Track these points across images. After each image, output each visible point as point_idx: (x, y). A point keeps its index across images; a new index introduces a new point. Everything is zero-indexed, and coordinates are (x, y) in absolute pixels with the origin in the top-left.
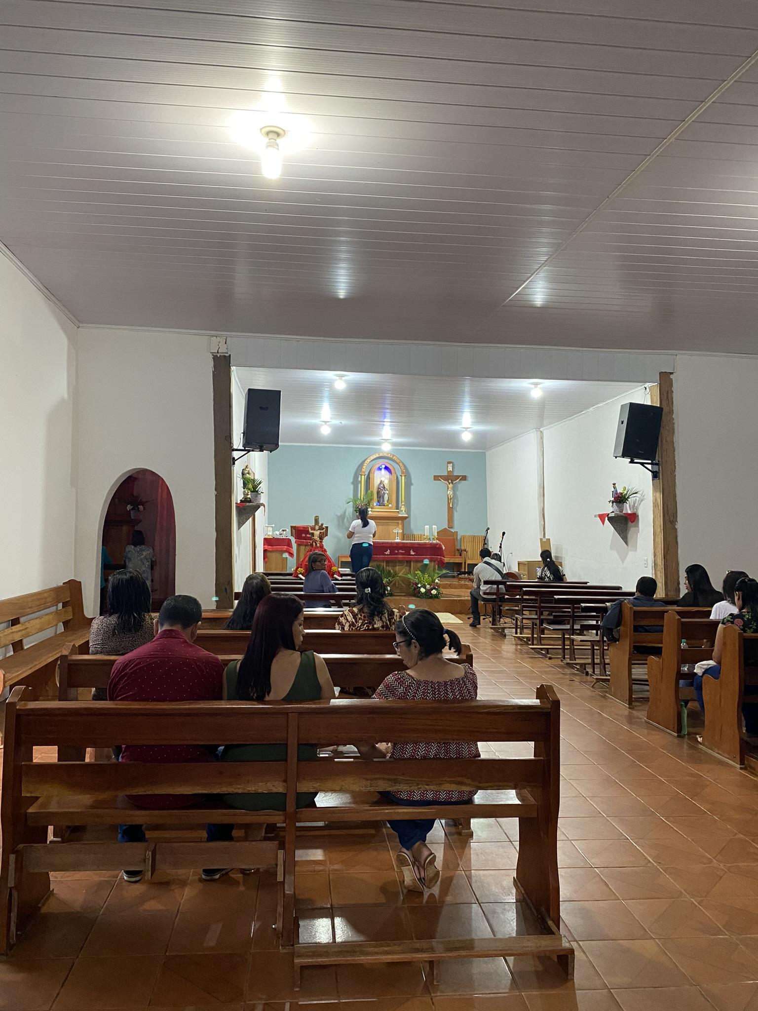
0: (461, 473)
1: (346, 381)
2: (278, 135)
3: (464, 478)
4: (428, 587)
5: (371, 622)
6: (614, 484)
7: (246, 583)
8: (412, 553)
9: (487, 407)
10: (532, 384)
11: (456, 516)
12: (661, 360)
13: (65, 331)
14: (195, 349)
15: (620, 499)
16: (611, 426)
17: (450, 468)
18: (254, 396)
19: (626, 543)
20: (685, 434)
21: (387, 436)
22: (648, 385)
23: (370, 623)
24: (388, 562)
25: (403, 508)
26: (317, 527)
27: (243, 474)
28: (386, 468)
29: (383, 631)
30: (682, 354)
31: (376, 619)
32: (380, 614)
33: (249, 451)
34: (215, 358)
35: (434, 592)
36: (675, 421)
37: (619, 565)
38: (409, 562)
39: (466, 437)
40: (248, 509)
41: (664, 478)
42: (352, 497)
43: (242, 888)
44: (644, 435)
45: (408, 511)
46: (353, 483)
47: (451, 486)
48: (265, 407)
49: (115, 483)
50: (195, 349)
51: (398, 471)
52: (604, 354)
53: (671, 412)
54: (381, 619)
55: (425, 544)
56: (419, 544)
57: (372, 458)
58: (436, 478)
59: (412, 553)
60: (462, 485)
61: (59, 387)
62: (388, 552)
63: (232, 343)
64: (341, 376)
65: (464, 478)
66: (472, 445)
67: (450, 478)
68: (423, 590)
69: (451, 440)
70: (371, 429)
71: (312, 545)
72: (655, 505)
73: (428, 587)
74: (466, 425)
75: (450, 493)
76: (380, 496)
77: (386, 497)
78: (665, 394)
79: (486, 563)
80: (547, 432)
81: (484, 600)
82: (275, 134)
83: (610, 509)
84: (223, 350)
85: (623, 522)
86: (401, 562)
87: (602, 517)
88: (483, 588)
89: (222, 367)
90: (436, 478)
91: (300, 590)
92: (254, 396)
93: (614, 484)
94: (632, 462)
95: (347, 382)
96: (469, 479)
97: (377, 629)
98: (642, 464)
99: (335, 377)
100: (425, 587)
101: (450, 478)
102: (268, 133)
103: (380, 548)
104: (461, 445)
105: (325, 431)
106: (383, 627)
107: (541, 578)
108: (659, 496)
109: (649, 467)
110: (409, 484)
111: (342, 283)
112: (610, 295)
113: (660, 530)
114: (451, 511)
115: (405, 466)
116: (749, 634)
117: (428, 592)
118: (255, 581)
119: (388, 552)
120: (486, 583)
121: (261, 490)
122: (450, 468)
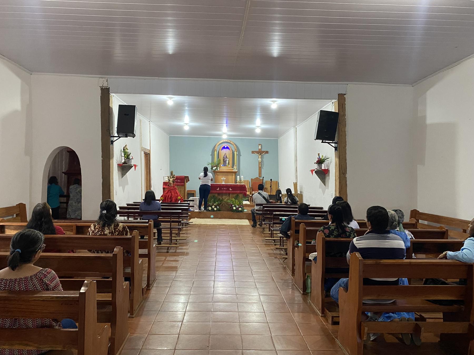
0: (266, 149)
1: (173, 101)
3: (267, 152)
4: (237, 206)
5: (103, 230)
6: (319, 154)
7: (34, 209)
8: (230, 189)
9: (268, 115)
10: (272, 101)
11: (263, 170)
12: (339, 87)
13: (18, 75)
14: (93, 84)
15: (320, 162)
17: (260, 148)
18: (121, 108)
19: (325, 185)
21: (225, 132)
22: (333, 101)
23: (102, 231)
24: (219, 194)
25: (235, 167)
26: (171, 177)
27: (124, 150)
28: (224, 148)
30: (351, 84)
31: (106, 228)
32: (109, 225)
33: (120, 137)
34: (102, 89)
35: (240, 209)
36: (347, 120)
38: (229, 194)
39: (258, 131)
42: (210, 162)
44: (329, 127)
46: (211, 155)
47: (260, 156)
48: (128, 113)
49: (51, 154)
50: (93, 84)
51: (232, 147)
52: (309, 84)
53: (344, 115)
54: (109, 228)
55: (238, 185)
56: (220, 185)
57: (220, 142)
58: (253, 152)
59: (230, 189)
60: (266, 156)
62: (218, 189)
63: (112, 81)
64: (171, 98)
65: (267, 152)
66: (261, 136)
67: (260, 152)
68: (234, 208)
70: (217, 127)
71: (169, 185)
72: (336, 165)
73: (237, 206)
74: (258, 125)
75: (260, 159)
76: (225, 162)
77: (227, 162)
78: (341, 106)
79: (259, 193)
81: (257, 214)
83: (316, 167)
84: (105, 85)
85: (322, 174)
86: (226, 194)
87: (312, 171)
88: (256, 208)
89: (105, 94)
90: (253, 152)
91: (138, 209)
92: (121, 108)
93: (319, 154)
94: (322, 142)
95: (173, 101)
96: (270, 152)
97: (106, 235)
98: (329, 143)
99: (168, 99)
100: (235, 207)
101: (260, 152)
103: (214, 187)
105: (186, 128)
106: (109, 233)
108: (337, 160)
109: (333, 145)
110: (239, 155)
111: (171, 43)
112: (308, 50)
113: (337, 178)
114: (260, 169)
115: (236, 145)
118: (38, 208)
119: (218, 189)
120: (257, 205)
121: (131, 157)
122: (260, 148)
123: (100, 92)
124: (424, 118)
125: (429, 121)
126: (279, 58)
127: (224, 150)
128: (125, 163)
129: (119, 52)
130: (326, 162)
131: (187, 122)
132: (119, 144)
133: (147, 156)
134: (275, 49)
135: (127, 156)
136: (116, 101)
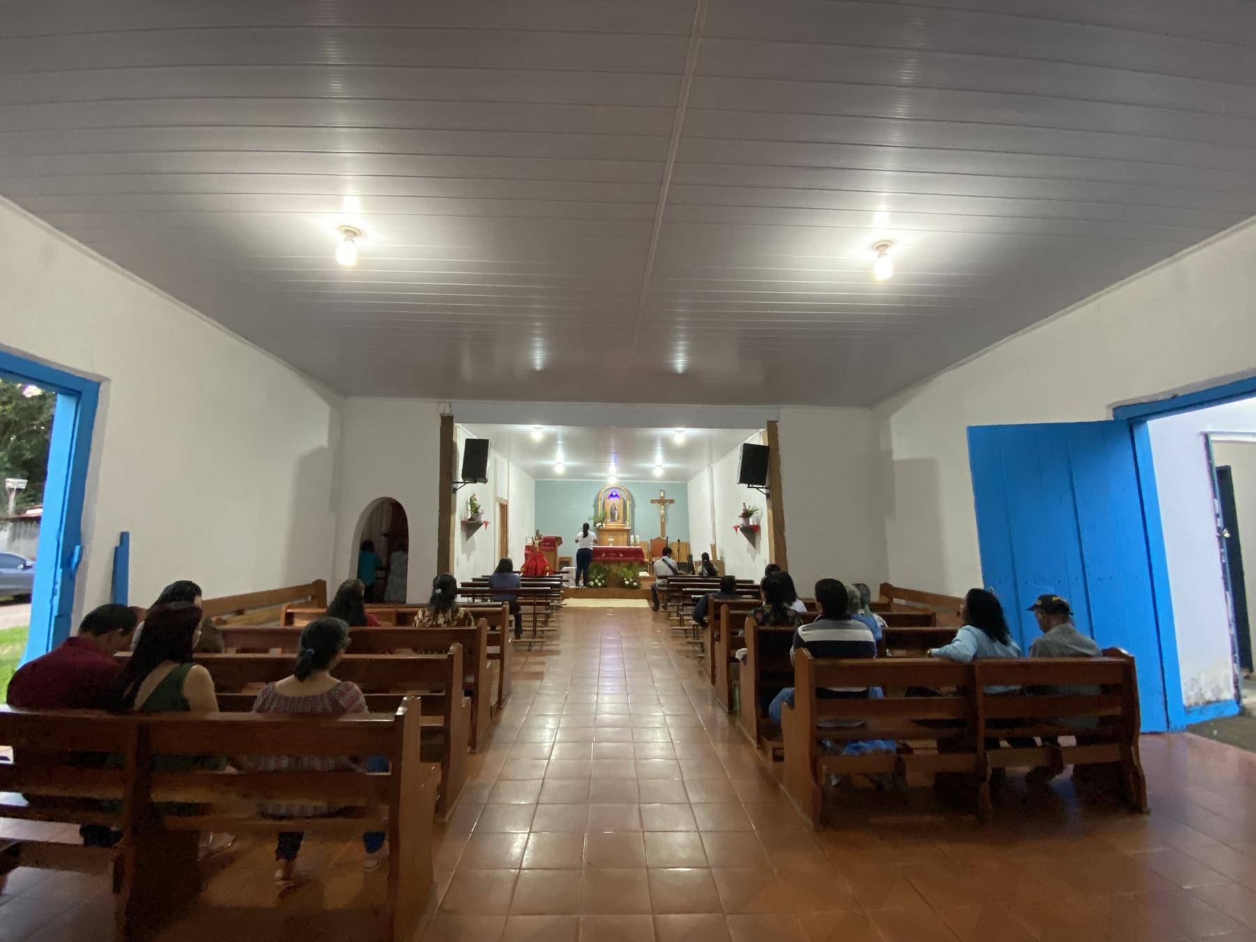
2: (355, 234)
3: (672, 501)
5: (435, 618)
12: (768, 412)
15: (747, 515)
16: (735, 460)
20: (789, 465)
21: (613, 474)
24: (604, 562)
29: (444, 627)
31: (440, 616)
32: (445, 611)
37: (748, 564)
40: (471, 526)
41: (775, 499)
43: (371, 863)
44: (757, 466)
45: (633, 524)
48: (478, 450)
50: (428, 412)
51: (623, 495)
58: (653, 501)
60: (671, 507)
61: (320, 438)
65: (672, 501)
67: (662, 501)
69: (646, 473)
74: (658, 465)
76: (613, 515)
80: (716, 468)
82: (352, 233)
83: (741, 522)
84: (448, 411)
85: (751, 532)
86: (614, 562)
87: (736, 528)
89: (447, 425)
90: (653, 501)
94: (1217, 516)
101: (662, 501)
102: (346, 231)
103: (598, 552)
104: (653, 478)
107: (701, 574)
110: (633, 506)
111: (538, 358)
114: (663, 524)
116: (767, 627)
117: (631, 584)
123: (439, 421)
124: (890, 452)
125: (896, 456)
126: (688, 373)
127: (612, 499)
128: (471, 519)
129: (467, 367)
130: (755, 515)
131: (560, 463)
132: (465, 492)
133: (504, 508)
134: (680, 363)
135: (475, 510)
136: (462, 434)
